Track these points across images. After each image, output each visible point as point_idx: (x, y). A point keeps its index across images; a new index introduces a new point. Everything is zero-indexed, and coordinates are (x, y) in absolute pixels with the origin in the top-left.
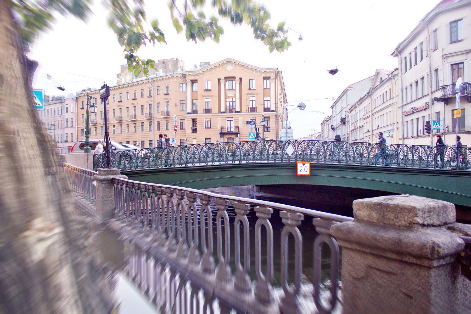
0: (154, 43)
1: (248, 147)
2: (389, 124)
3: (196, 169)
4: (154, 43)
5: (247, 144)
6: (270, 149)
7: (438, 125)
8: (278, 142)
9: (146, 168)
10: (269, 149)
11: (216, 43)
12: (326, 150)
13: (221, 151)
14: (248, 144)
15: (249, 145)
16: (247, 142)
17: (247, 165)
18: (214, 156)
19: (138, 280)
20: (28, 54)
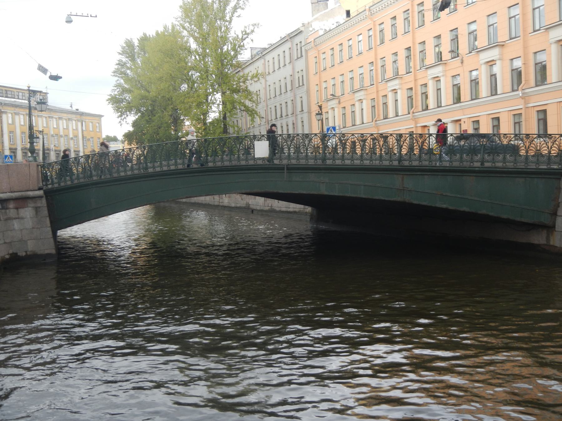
0: (246, 34)
1: (248, 143)
2: (530, 108)
3: (336, 168)
4: (246, 34)
5: (391, 138)
6: (310, 146)
8: (416, 137)
9: (234, 163)
10: (529, 147)
11: (45, 75)
12: (529, 147)
13: (299, 146)
14: (393, 138)
15: (337, 139)
16: (391, 135)
17: (419, 168)
18: (308, 152)
19: (550, 371)
20: (115, 69)
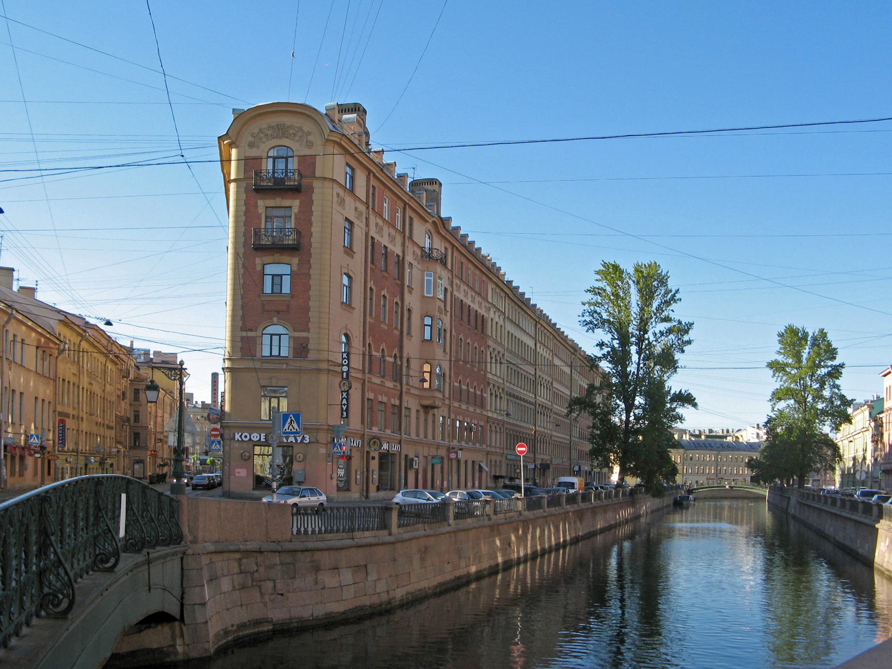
7: (218, 446)
